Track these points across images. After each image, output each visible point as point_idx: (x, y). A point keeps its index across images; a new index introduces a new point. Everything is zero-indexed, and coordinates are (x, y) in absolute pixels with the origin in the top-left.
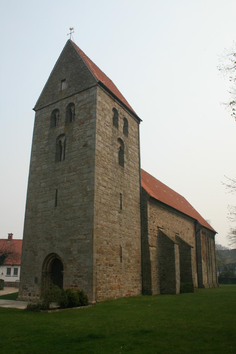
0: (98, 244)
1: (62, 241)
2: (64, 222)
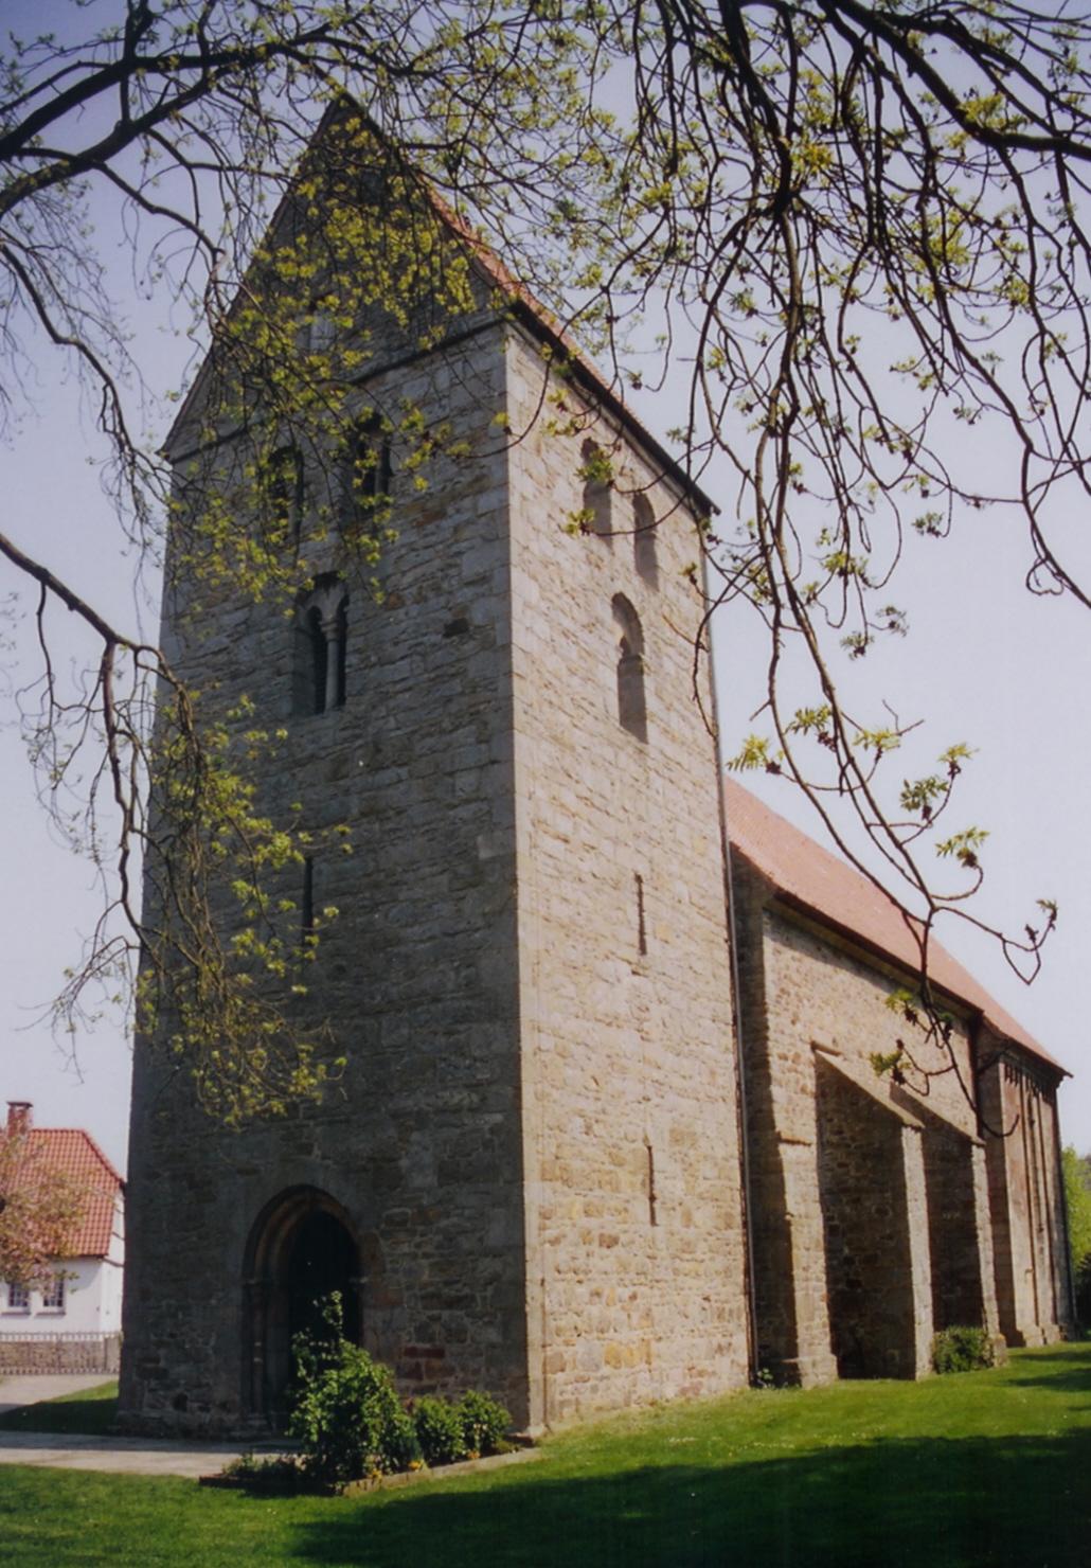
0: (547, 1131)
1: (348, 1121)
2: (357, 1021)
